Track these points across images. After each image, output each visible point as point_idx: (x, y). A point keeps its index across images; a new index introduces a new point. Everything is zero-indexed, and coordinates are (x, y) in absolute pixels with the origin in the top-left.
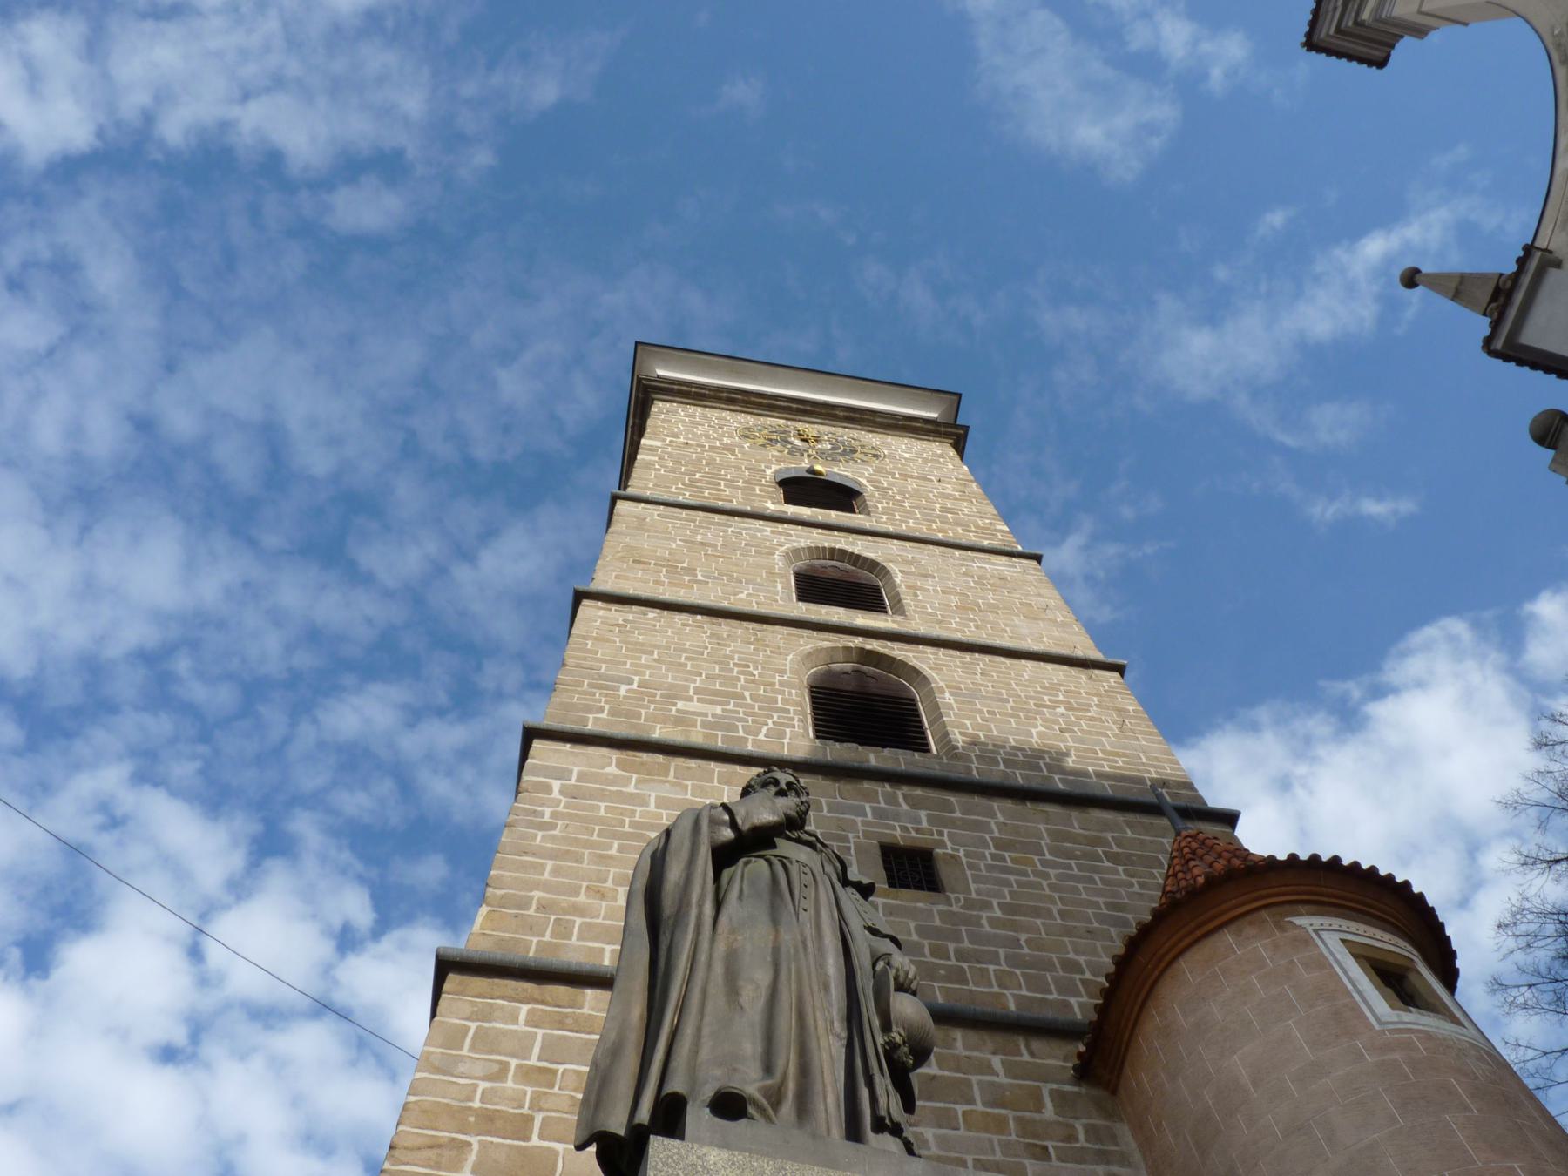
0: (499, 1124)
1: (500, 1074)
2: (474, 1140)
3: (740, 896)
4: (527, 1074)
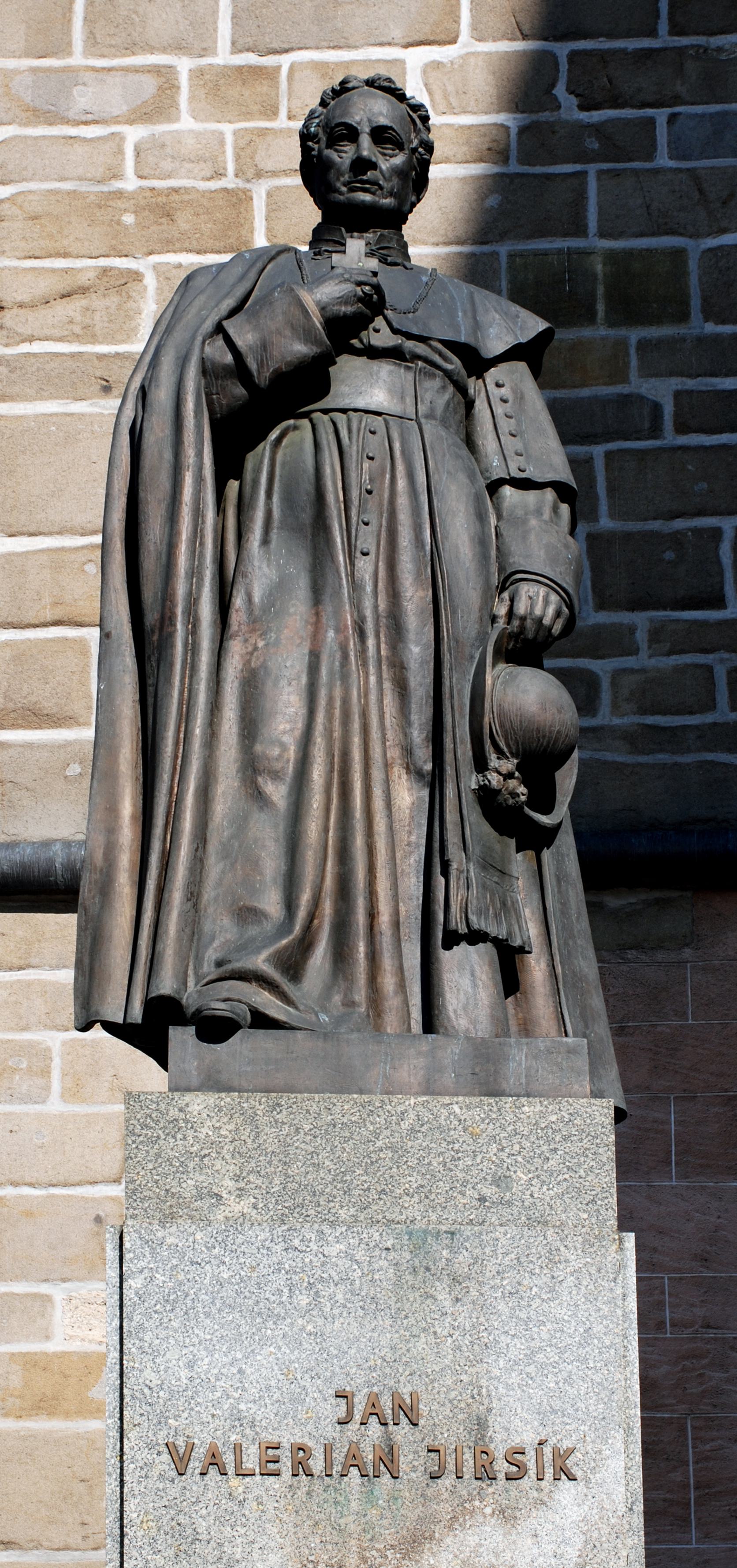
0: (184, 221)
1: (158, 107)
2: (142, 265)
3: (265, 541)
4: (217, 88)
